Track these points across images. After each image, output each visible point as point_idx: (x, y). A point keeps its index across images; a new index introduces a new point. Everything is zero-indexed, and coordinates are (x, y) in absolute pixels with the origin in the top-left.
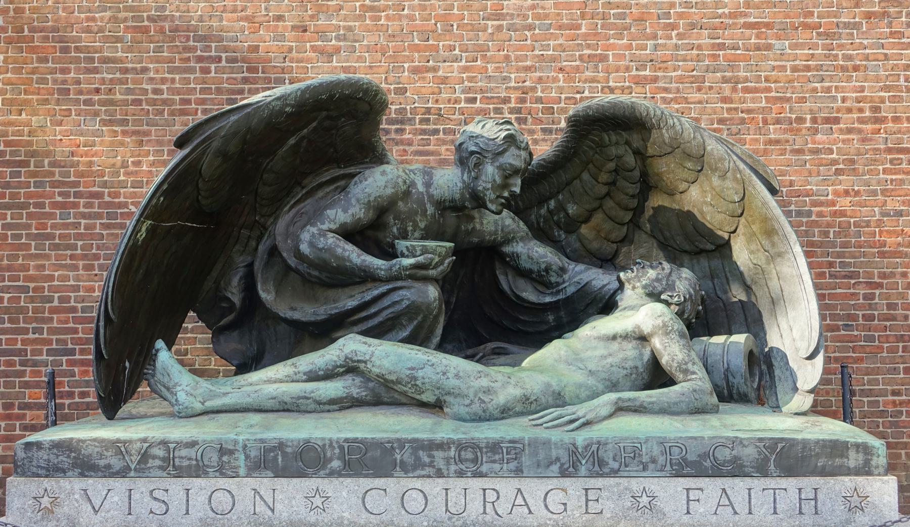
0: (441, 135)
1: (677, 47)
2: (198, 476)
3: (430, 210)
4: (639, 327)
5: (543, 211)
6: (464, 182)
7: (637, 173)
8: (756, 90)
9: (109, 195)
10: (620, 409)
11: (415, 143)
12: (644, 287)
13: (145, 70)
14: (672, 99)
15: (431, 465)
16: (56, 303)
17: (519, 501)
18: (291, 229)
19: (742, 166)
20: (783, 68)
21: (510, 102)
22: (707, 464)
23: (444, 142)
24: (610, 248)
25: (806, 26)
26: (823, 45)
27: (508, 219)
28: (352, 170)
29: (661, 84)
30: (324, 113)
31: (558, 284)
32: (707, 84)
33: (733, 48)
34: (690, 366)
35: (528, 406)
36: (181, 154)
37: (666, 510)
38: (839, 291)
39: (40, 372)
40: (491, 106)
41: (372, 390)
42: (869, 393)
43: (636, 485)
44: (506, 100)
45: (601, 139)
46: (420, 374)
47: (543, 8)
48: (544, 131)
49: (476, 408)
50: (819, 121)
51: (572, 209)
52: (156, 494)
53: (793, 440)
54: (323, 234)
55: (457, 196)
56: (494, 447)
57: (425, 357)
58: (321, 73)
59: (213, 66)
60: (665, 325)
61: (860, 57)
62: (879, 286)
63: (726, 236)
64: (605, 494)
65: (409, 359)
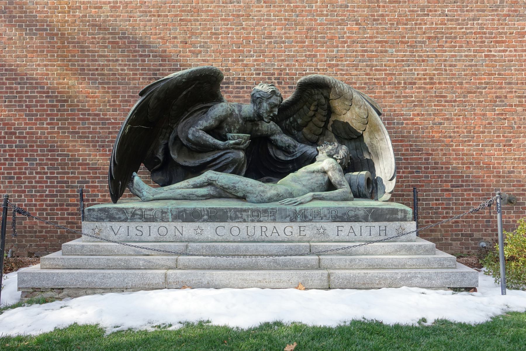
0: (245, 89)
1: (347, 51)
2: (154, 222)
3: (241, 121)
4: (323, 168)
5: (288, 122)
6: (254, 110)
7: (326, 106)
8: (380, 70)
9: (103, 115)
10: (314, 198)
11: (234, 92)
12: (327, 152)
13: (117, 60)
14: (344, 74)
15: (241, 217)
16: (81, 161)
17: (275, 231)
18: (184, 129)
19: (367, 103)
20: (392, 61)
21: (274, 75)
22: (345, 217)
23: (246, 92)
24: (315, 138)
25: (402, 42)
26: (410, 50)
27: (272, 125)
28: (208, 105)
29: (340, 68)
30: (198, 82)
31: (293, 152)
32: (360, 67)
33: (371, 52)
34: (342, 183)
35: (279, 198)
36: (140, 100)
37: (329, 234)
38: (414, 157)
39: (74, 190)
40: (267, 77)
41: (218, 192)
42: (426, 200)
43: (318, 225)
44: (273, 74)
45: (311, 92)
46: (237, 185)
47: (289, 34)
48: (289, 87)
49: (259, 198)
50: (407, 84)
51: (299, 121)
52: (138, 228)
53: (378, 208)
54: (197, 131)
55: (252, 116)
56: (265, 211)
57: (239, 179)
58: (195, 64)
59: (146, 59)
60: (333, 167)
61: (425, 56)
62: (431, 154)
63: (361, 132)
64: (307, 228)
65: (233, 180)
